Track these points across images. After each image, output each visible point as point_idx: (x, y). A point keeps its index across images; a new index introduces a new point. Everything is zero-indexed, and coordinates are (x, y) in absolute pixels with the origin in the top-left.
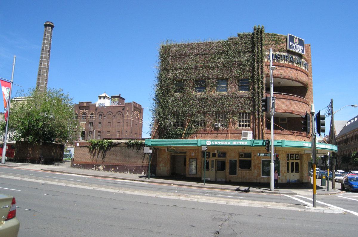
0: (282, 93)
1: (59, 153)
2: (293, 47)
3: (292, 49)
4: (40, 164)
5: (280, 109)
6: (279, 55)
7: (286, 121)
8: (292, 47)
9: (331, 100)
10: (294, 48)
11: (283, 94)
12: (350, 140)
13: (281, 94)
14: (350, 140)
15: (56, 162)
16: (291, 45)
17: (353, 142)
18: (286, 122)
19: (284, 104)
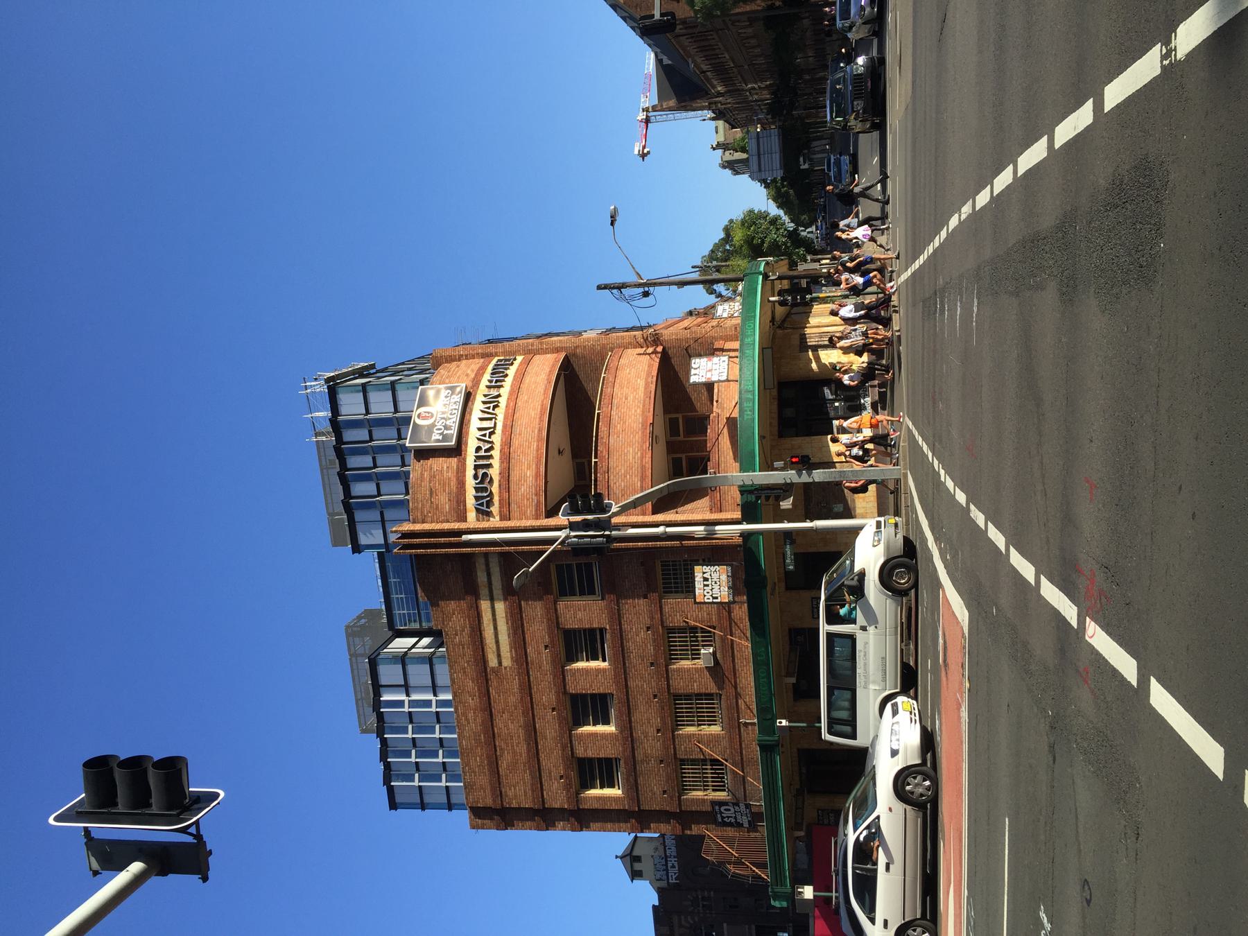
0: (593, 460)
1: (695, 896)
2: (446, 427)
3: (452, 432)
4: (574, 595)
5: (643, 467)
6: (476, 477)
7: (681, 458)
8: (446, 432)
9: (599, 288)
10: (448, 423)
11: (596, 457)
12: (717, 61)
13: (596, 462)
14: (717, 61)
15: (620, 712)
16: (441, 438)
17: (723, 54)
18: (680, 416)
19: (626, 455)
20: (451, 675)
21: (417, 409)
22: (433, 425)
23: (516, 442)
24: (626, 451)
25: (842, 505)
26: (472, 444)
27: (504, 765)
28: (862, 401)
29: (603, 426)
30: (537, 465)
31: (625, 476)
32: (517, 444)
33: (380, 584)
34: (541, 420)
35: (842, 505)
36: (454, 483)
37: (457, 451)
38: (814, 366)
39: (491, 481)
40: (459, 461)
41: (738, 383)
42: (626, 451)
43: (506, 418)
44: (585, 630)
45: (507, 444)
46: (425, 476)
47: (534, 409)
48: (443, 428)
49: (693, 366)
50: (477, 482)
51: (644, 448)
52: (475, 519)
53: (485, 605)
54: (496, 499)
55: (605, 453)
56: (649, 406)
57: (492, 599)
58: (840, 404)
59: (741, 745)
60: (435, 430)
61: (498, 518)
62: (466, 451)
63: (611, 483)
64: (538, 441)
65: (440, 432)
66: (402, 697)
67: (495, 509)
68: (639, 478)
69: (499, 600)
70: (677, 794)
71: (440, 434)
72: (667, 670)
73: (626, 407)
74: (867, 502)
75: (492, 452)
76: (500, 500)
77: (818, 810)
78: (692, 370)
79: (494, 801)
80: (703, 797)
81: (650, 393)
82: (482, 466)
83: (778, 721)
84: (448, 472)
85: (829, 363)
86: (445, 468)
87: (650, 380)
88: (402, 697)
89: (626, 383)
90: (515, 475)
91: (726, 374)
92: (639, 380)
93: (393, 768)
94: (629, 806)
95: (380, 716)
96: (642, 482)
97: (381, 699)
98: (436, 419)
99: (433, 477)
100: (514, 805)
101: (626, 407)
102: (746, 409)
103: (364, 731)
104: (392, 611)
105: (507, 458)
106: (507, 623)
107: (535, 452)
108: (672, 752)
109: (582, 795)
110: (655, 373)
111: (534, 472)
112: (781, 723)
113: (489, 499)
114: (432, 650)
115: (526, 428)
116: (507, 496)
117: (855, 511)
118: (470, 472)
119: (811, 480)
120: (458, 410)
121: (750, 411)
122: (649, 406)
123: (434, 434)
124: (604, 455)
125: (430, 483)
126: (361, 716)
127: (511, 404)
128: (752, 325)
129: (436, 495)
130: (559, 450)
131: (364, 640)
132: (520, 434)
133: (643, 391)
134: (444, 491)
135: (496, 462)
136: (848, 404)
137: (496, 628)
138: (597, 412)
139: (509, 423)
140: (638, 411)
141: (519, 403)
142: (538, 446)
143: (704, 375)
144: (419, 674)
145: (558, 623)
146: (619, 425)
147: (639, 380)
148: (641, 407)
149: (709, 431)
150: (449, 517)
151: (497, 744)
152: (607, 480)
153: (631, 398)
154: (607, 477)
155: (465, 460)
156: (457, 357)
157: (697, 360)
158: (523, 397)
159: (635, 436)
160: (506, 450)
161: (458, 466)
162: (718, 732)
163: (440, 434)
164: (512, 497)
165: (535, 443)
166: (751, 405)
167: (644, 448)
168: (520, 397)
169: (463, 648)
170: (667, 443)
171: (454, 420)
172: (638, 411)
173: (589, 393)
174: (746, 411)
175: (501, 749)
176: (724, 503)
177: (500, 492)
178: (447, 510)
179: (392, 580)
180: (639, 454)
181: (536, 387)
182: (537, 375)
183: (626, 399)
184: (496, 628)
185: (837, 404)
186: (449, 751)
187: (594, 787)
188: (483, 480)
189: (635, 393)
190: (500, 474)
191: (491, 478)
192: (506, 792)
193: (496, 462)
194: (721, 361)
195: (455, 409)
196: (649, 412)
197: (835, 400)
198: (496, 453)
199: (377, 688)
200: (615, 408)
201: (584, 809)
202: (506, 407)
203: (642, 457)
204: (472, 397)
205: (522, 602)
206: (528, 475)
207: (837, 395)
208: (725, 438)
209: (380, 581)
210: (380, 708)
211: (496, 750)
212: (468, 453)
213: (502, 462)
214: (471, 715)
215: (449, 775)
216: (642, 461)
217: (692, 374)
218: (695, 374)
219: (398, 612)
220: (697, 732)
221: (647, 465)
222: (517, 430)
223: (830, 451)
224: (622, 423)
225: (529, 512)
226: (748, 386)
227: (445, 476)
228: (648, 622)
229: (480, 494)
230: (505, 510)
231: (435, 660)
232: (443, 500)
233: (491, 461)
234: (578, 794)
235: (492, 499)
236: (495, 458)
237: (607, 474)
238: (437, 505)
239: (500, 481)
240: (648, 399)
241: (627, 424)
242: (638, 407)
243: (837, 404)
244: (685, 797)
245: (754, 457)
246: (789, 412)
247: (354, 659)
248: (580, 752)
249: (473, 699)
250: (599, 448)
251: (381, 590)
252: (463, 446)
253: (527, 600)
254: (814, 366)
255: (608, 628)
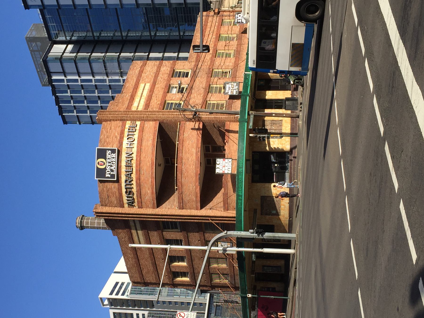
0: (176, 187)
2: (112, 171)
8: (112, 173)
16: (110, 176)
20: (121, 249)
21: (97, 160)
22: (105, 169)
23: (142, 178)
24: (189, 185)
25: (275, 211)
26: (123, 178)
27: (144, 272)
28: (286, 165)
29: (179, 174)
30: (152, 188)
31: (189, 195)
32: (143, 179)
33: (41, 17)
34: (152, 169)
35: (275, 211)
36: (117, 194)
37: (118, 181)
38: (267, 148)
39: (133, 194)
40: (118, 185)
41: (237, 161)
42: (189, 185)
43: (136, 166)
44: (174, 240)
45: (138, 179)
46: (105, 189)
47: (149, 162)
48: (110, 171)
49: (217, 163)
50: (127, 194)
51: (197, 185)
52: (128, 207)
53: (134, 232)
54: (136, 201)
55: (180, 186)
56: (198, 165)
57: (136, 230)
58: (277, 165)
59: (234, 271)
60: (107, 172)
61: (137, 207)
62: (121, 181)
63: (184, 198)
64: (152, 178)
65: (109, 173)
66: (63, 77)
67: (136, 204)
68: (195, 196)
69: (139, 230)
70: (210, 282)
71: (110, 174)
72: (209, 268)
73: (188, 165)
74: (285, 211)
75: (132, 182)
76: (137, 201)
77: (261, 287)
78: (217, 165)
79: (141, 281)
80: (219, 282)
81: (198, 158)
82: (129, 182)
83: (248, 295)
84: (114, 189)
85: (274, 148)
86: (113, 187)
87: (198, 150)
88: (63, 77)
89: (187, 150)
90: (143, 192)
91: (230, 170)
92: (193, 149)
93: (56, 87)
94: (192, 284)
95: (53, 87)
96: (196, 198)
97: (52, 78)
98: (106, 166)
99: (108, 191)
100: (149, 281)
101: (188, 165)
102: (239, 203)
103: (44, 85)
104: (45, 17)
105: (139, 185)
106: (143, 236)
107: (151, 183)
108: (208, 271)
109: (174, 280)
110: (200, 145)
111: (151, 191)
112: (249, 295)
113: (133, 201)
114: (75, 54)
115: (146, 171)
116: (141, 200)
117: (280, 213)
118: (124, 190)
119: (263, 238)
120: (115, 162)
121: (241, 204)
122: (198, 165)
123: (106, 174)
124: (180, 187)
125: (107, 193)
126: (41, 79)
127: (138, 159)
128: (242, 161)
129: (110, 197)
130: (159, 164)
131: (36, 51)
132: (144, 174)
133: (195, 156)
134: (114, 196)
135: (134, 186)
136: (281, 165)
137: (138, 237)
138: (176, 165)
139: (138, 169)
140: (194, 167)
141: (142, 158)
142: (152, 181)
143: (222, 168)
144: (70, 67)
145: (163, 238)
146: (186, 173)
147: (193, 149)
148: (195, 165)
149: (223, 179)
150: (117, 205)
151: (141, 267)
152: (181, 197)
153: (190, 159)
154: (181, 196)
155: (121, 185)
156: (109, 120)
157: (219, 160)
158: (143, 155)
159: (192, 179)
160: (138, 182)
161: (118, 186)
162: (226, 267)
163: (110, 174)
164: (142, 200)
165: (151, 179)
166: (241, 201)
167: (197, 185)
168: (142, 155)
169: (126, 242)
170: (204, 154)
171: (114, 167)
172: (194, 167)
173: (170, 136)
174: (239, 204)
175: (143, 268)
176: (229, 207)
177: (137, 199)
178: (116, 203)
179: (47, 16)
180: (195, 187)
181: (148, 149)
182: (148, 140)
183: (188, 160)
184: (138, 237)
185: (276, 165)
186: (89, 101)
187: (179, 277)
188: (129, 192)
189: (192, 157)
190: (137, 191)
191: (133, 193)
192: (145, 279)
193: (134, 186)
194: (229, 161)
195: (114, 161)
196: (198, 168)
197: (276, 163)
198: (134, 182)
199: (49, 74)
200: (184, 164)
201: (175, 284)
202: (136, 160)
203: (196, 188)
204: (120, 153)
205: (149, 232)
206: (149, 192)
207: (276, 160)
208: (230, 183)
209: (40, 16)
210: (56, 94)
211: (141, 268)
212: (122, 182)
213: (137, 187)
214: (130, 259)
215: (88, 101)
216: (196, 190)
217: (217, 167)
218: (218, 168)
219: (53, 32)
220: (218, 267)
221: (198, 192)
222: (142, 172)
223: (272, 192)
224: (187, 172)
225: (150, 206)
226: (240, 193)
227: (113, 191)
228: (199, 239)
229: (129, 199)
230: (140, 205)
231: (77, 61)
232: (114, 199)
233: (132, 186)
234: (173, 280)
235: (134, 200)
236: (134, 184)
237: (181, 195)
238: (111, 201)
239: (137, 194)
240: (197, 161)
241: (189, 173)
242: (194, 165)
243: (276, 165)
244: (213, 282)
245: (242, 222)
246: (257, 167)
247: (33, 53)
248: (173, 270)
249: (131, 255)
250: (178, 184)
251: (42, 20)
252: (120, 179)
253: (151, 231)
254: (267, 148)
255: (183, 239)
